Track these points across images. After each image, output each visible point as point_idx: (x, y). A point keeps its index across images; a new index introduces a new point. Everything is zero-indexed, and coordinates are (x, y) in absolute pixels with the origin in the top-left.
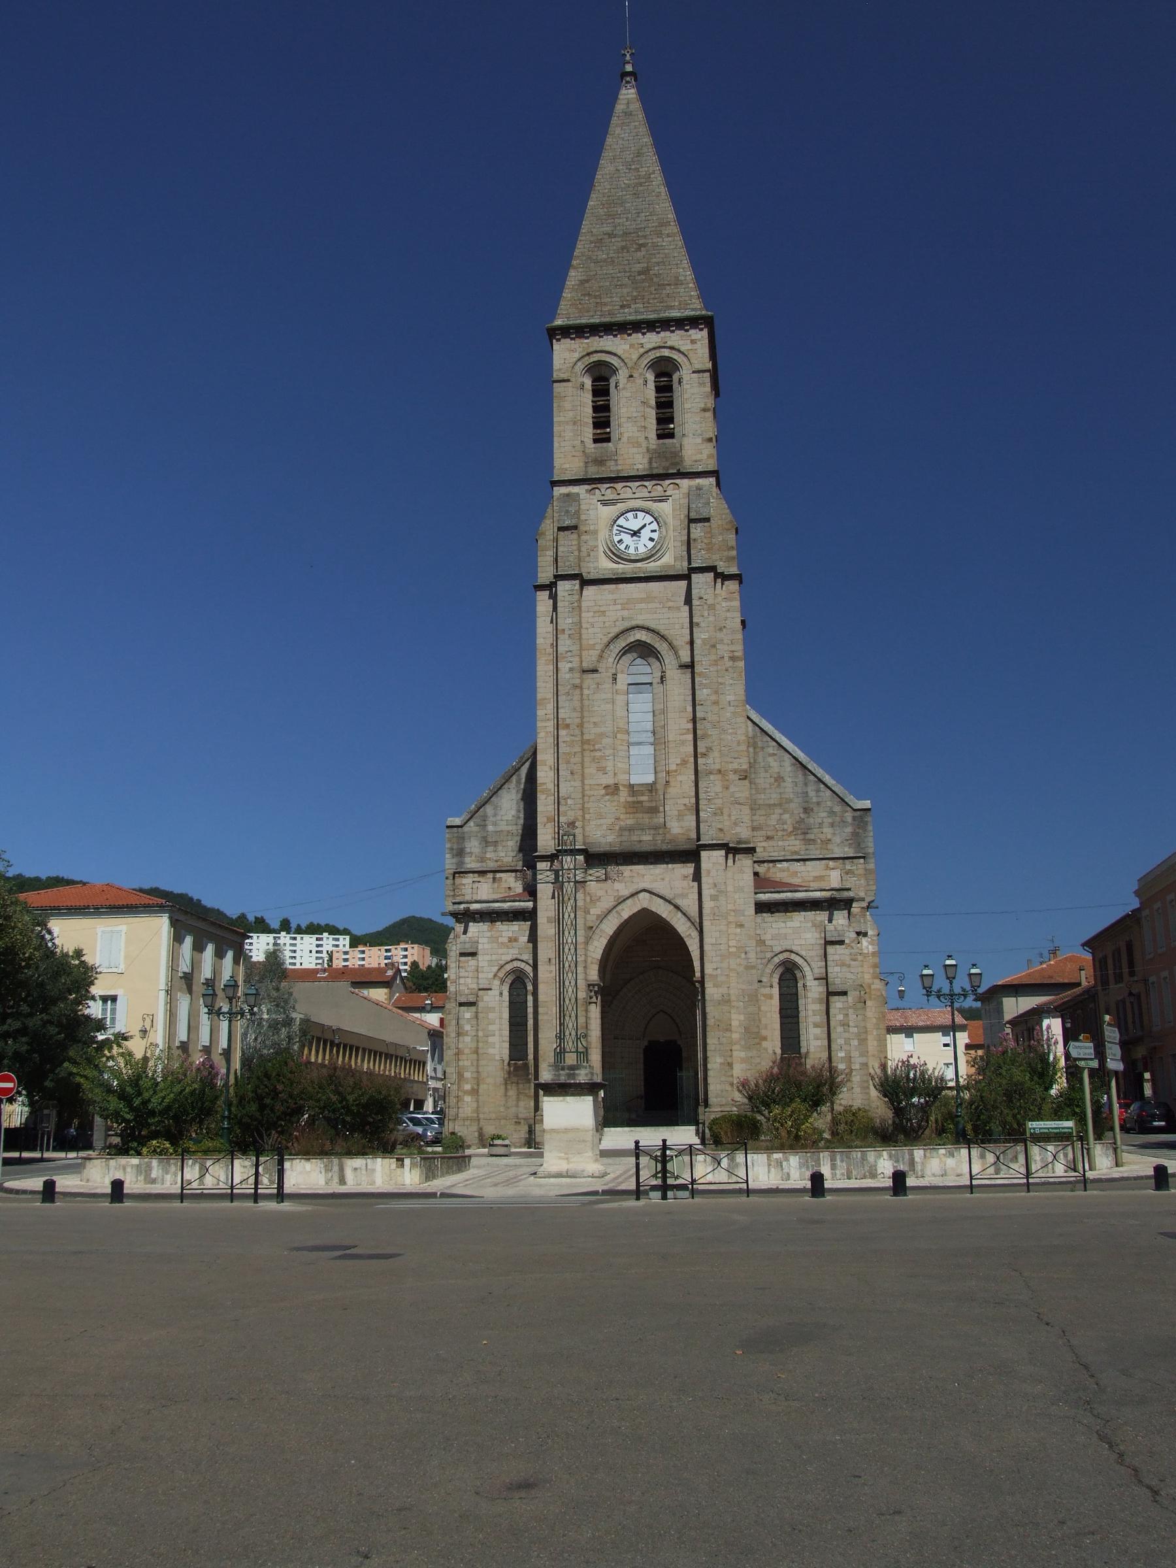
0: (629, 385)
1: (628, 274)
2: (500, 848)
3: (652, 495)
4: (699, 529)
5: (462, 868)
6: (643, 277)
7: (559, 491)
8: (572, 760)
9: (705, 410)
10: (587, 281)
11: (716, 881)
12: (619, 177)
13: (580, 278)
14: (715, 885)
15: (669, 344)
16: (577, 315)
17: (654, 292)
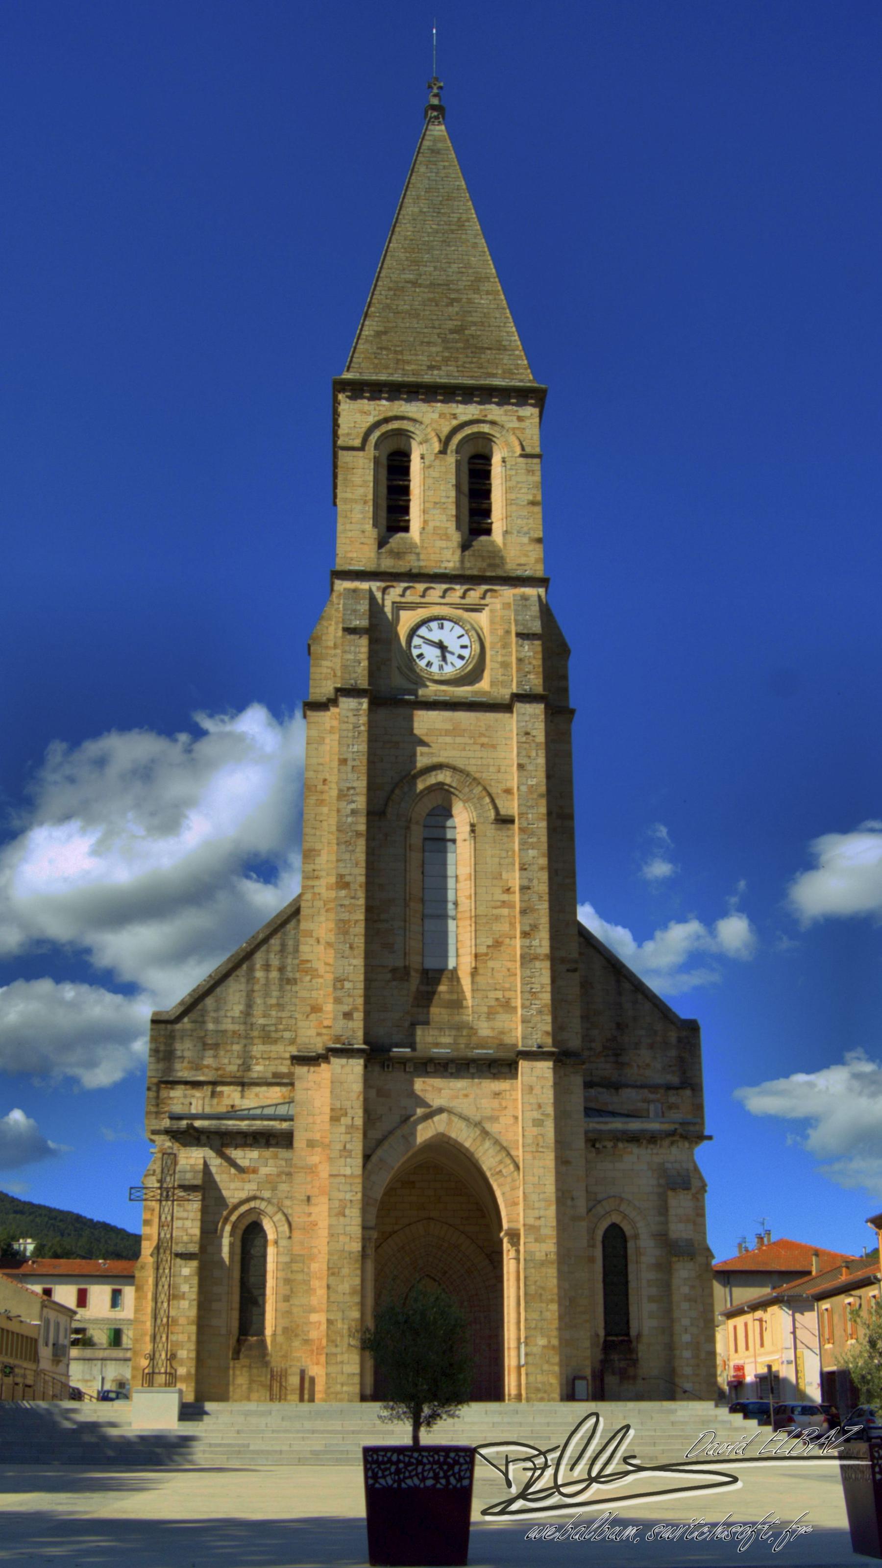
0: (437, 463)
1: (438, 331)
2: (222, 1053)
3: (463, 601)
4: (527, 647)
5: (170, 1076)
6: (456, 336)
7: (342, 585)
8: (351, 930)
9: (533, 503)
10: (385, 333)
11: (540, 1101)
12: (425, 221)
13: (376, 328)
14: (540, 1106)
15: (490, 418)
16: (372, 371)
17: (470, 355)
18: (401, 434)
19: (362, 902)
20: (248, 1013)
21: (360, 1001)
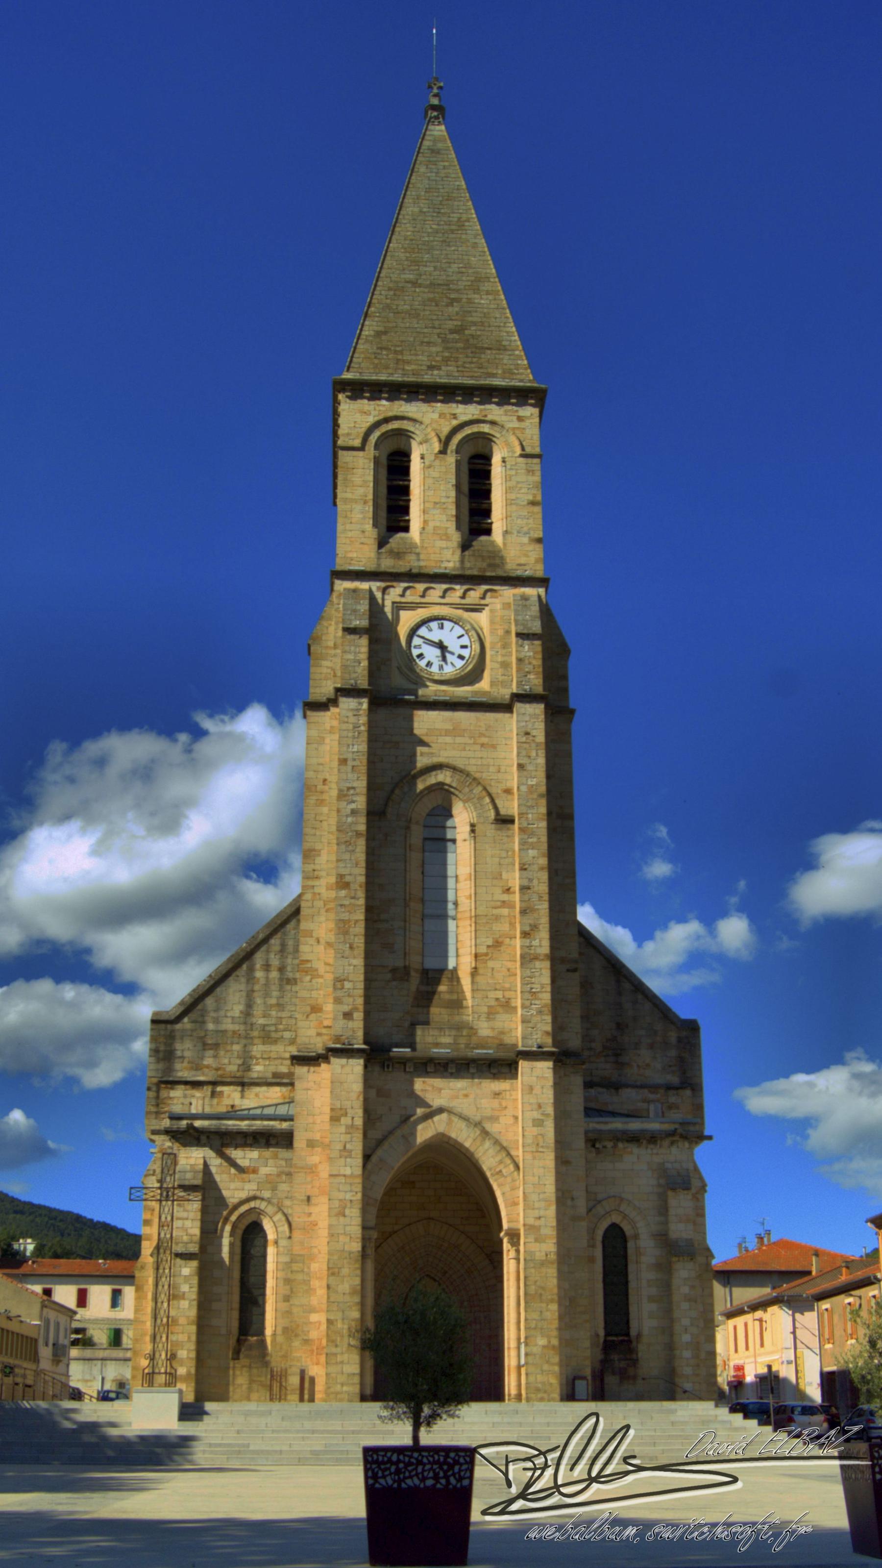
0: (437, 463)
1: (438, 331)
2: (222, 1053)
3: (463, 601)
4: (527, 647)
5: (170, 1076)
6: (456, 336)
7: (342, 585)
8: (351, 930)
9: (533, 503)
10: (385, 333)
11: (540, 1101)
12: (425, 221)
13: (376, 328)
14: (540, 1106)
15: (490, 418)
16: (372, 371)
17: (470, 355)
18: (401, 434)
19: (362, 902)
20: (248, 1013)
21: (360, 1001)
